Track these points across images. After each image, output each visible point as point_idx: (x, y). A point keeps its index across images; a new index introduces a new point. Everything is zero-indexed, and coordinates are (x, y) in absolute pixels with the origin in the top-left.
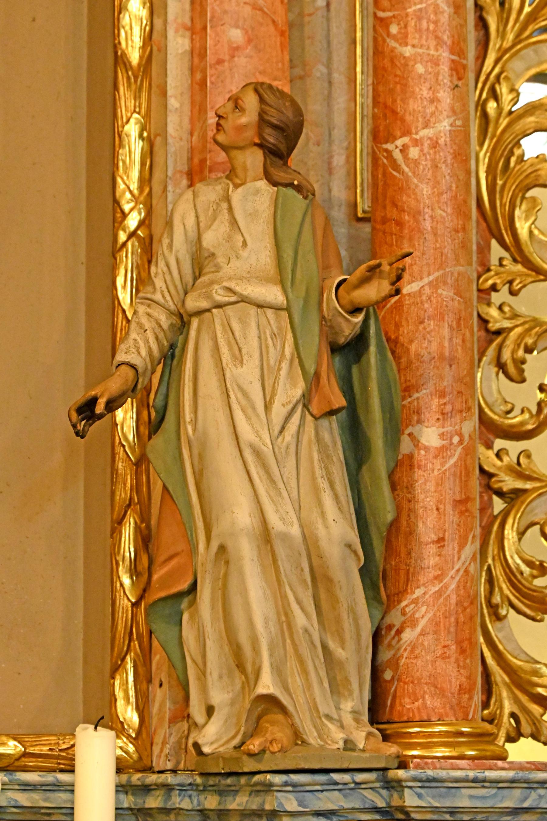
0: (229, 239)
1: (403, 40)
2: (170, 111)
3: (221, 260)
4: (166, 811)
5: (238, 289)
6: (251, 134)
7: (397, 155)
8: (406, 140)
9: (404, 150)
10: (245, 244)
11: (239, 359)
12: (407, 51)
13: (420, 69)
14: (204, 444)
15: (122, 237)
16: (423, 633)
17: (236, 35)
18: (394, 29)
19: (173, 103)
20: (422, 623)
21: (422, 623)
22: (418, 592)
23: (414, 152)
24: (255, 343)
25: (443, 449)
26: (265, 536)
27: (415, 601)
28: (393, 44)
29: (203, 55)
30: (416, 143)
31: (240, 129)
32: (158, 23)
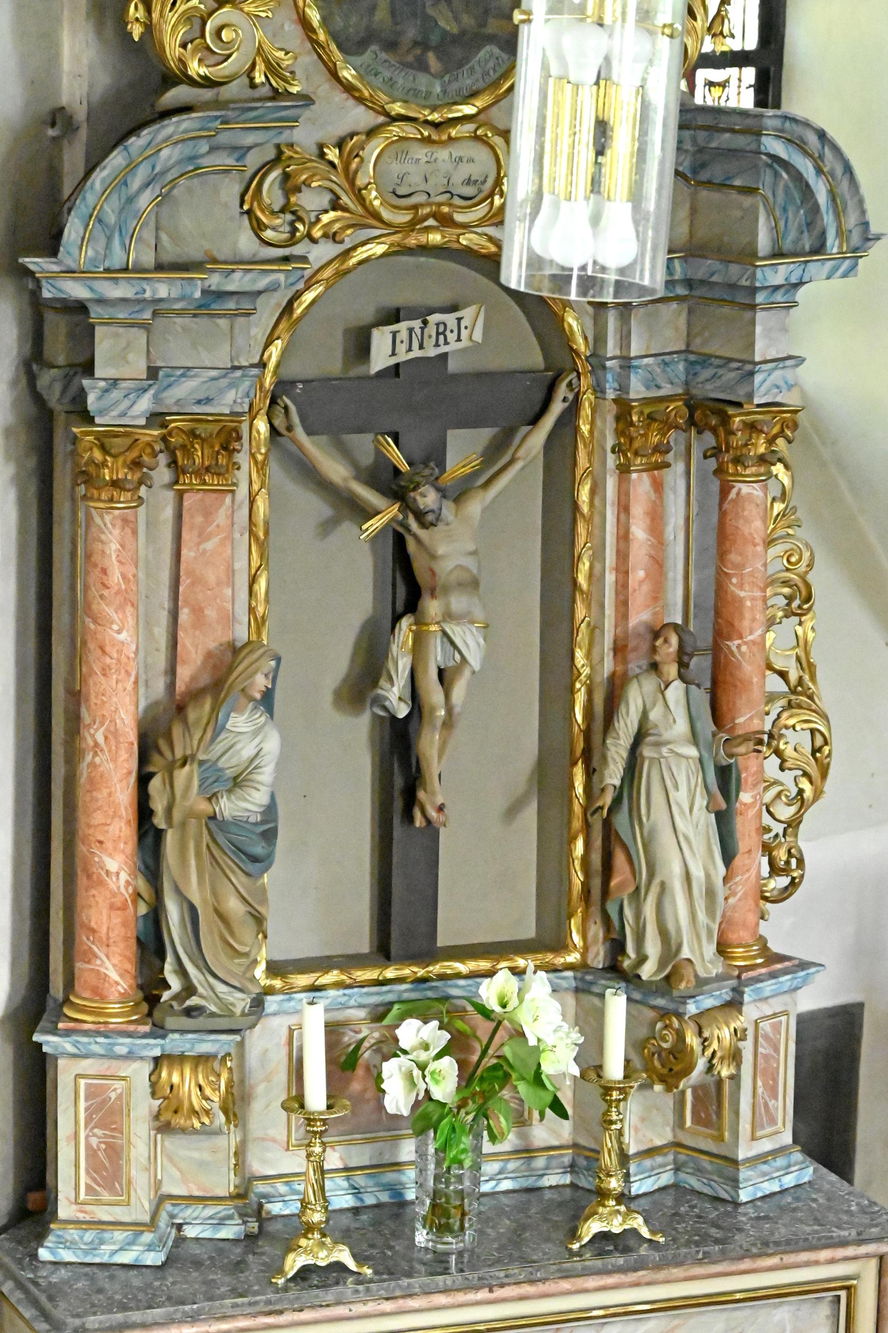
0: (665, 716)
1: (741, 587)
2: (126, 148)
3: (662, 730)
4: (267, 600)
5: (676, 750)
6: (674, 656)
7: (734, 649)
8: (739, 642)
9: (739, 647)
10: (675, 721)
11: (676, 787)
12: (742, 594)
13: (748, 603)
14: (653, 831)
15: (578, 685)
16: (740, 900)
17: (641, 574)
18: (734, 580)
19: (607, 612)
20: (739, 894)
21: (739, 894)
22: (738, 879)
23: (744, 648)
24: (685, 778)
25: (753, 803)
26: (688, 877)
27: (736, 883)
28: (733, 588)
29: (625, 586)
30: (746, 643)
31: (668, 654)
32: (598, 566)
